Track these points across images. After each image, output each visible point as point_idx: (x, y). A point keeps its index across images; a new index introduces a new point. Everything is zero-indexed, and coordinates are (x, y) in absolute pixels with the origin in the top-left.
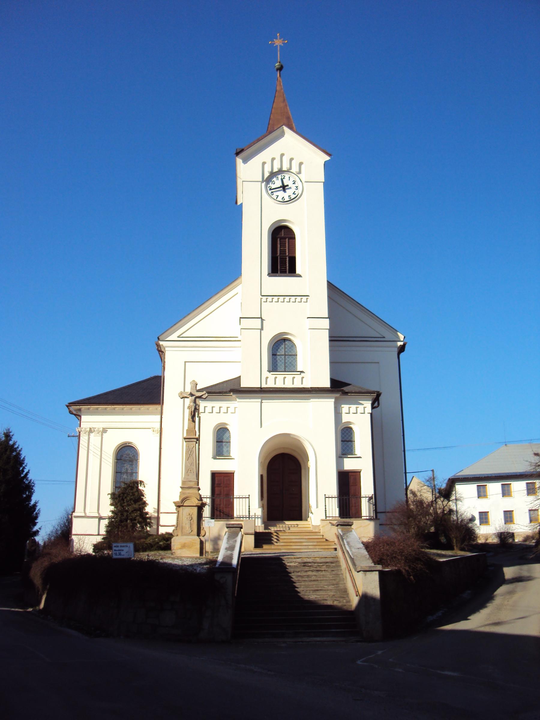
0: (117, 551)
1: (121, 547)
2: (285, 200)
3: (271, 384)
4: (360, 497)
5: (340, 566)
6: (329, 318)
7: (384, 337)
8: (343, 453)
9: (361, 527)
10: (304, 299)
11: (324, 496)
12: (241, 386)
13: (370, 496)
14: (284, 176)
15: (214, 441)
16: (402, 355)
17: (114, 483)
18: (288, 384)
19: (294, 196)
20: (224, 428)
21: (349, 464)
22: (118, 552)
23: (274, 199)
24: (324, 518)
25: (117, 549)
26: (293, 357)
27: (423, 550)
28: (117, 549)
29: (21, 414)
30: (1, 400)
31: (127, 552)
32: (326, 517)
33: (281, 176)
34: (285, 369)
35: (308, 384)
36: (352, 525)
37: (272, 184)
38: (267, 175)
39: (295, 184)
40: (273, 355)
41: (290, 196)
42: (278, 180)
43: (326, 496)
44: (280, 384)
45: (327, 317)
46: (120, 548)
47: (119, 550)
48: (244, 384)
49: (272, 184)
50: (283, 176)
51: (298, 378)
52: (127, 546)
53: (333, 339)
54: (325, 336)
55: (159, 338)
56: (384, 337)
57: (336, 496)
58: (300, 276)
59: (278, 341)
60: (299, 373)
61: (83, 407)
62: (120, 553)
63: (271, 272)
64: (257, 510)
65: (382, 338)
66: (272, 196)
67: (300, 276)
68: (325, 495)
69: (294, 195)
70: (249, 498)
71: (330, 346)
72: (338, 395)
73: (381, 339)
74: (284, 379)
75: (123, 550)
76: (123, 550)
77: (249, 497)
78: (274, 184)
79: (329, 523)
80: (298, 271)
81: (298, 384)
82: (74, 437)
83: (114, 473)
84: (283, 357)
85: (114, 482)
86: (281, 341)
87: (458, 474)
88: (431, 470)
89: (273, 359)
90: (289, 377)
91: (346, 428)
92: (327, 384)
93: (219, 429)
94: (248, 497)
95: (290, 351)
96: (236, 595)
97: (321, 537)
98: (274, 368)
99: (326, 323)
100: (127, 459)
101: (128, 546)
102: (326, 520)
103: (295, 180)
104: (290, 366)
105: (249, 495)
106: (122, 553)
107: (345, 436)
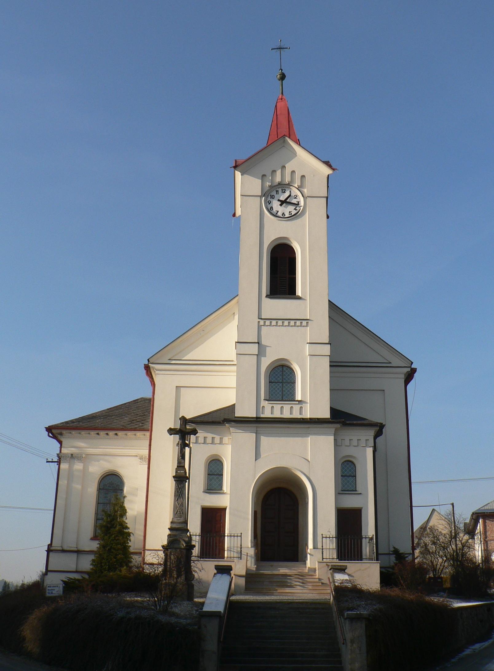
0: (50, 590)
1: (53, 587)
2: (285, 217)
3: (267, 414)
4: (361, 538)
5: (229, 531)
6: (330, 344)
7: (391, 363)
8: (344, 488)
9: (360, 570)
10: (304, 323)
11: (321, 535)
12: (236, 416)
13: (370, 537)
14: (284, 190)
15: (206, 474)
16: (378, 440)
17: (95, 515)
18: (286, 415)
19: (296, 212)
20: (216, 460)
21: (351, 502)
22: (50, 591)
23: (274, 214)
24: (321, 560)
25: (50, 589)
26: (291, 385)
27: (435, 599)
28: (50, 589)
29: (28, 452)
30: (1, 434)
31: (57, 591)
32: (323, 559)
33: (282, 189)
34: (282, 397)
35: (307, 415)
36: (346, 569)
37: (271, 198)
38: (267, 188)
39: (297, 198)
40: (270, 382)
41: (291, 212)
42: (278, 194)
43: (323, 536)
44: (277, 414)
45: (327, 342)
46: (52, 588)
47: (51, 590)
48: (239, 413)
49: (272, 199)
50: (284, 190)
51: (296, 408)
52: (58, 587)
53: (333, 365)
54: (326, 363)
55: (150, 360)
56: (391, 363)
57: (334, 536)
58: (299, 298)
59: (276, 367)
60: (297, 403)
61: (64, 432)
62: (52, 592)
63: (269, 294)
64: (249, 549)
65: (389, 363)
66: (271, 211)
67: (299, 298)
68: (322, 535)
69: (295, 210)
70: (241, 536)
71: (331, 372)
72: (338, 426)
73: (388, 365)
74: (281, 408)
75: (54, 590)
76: (54, 590)
77: (241, 535)
78: (274, 198)
79: (325, 564)
80: (299, 292)
81: (296, 415)
82: (53, 463)
83: (96, 504)
84: (281, 385)
85: (95, 514)
86: (279, 367)
87: (485, 508)
88: (451, 504)
89: (270, 391)
90: (287, 407)
91: (347, 462)
92: (327, 415)
93: (210, 461)
94: (240, 535)
95: (289, 379)
96: (352, 540)
97: (317, 580)
98: (272, 397)
99: (327, 350)
100: (110, 488)
101: (59, 586)
102: (322, 561)
103: (296, 194)
104: (288, 395)
105: (241, 534)
106: (54, 592)
107: (346, 470)
